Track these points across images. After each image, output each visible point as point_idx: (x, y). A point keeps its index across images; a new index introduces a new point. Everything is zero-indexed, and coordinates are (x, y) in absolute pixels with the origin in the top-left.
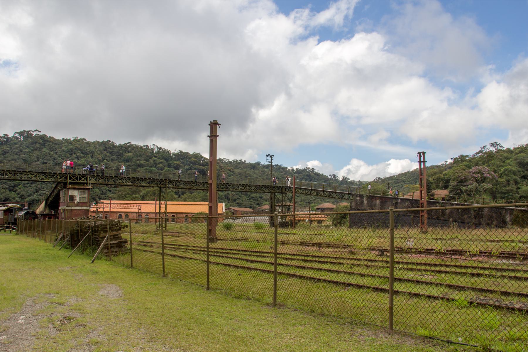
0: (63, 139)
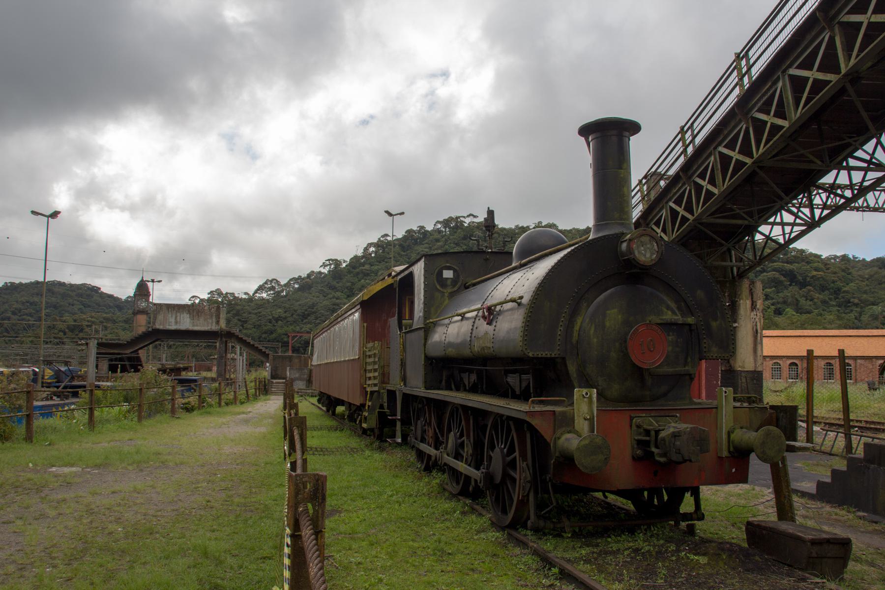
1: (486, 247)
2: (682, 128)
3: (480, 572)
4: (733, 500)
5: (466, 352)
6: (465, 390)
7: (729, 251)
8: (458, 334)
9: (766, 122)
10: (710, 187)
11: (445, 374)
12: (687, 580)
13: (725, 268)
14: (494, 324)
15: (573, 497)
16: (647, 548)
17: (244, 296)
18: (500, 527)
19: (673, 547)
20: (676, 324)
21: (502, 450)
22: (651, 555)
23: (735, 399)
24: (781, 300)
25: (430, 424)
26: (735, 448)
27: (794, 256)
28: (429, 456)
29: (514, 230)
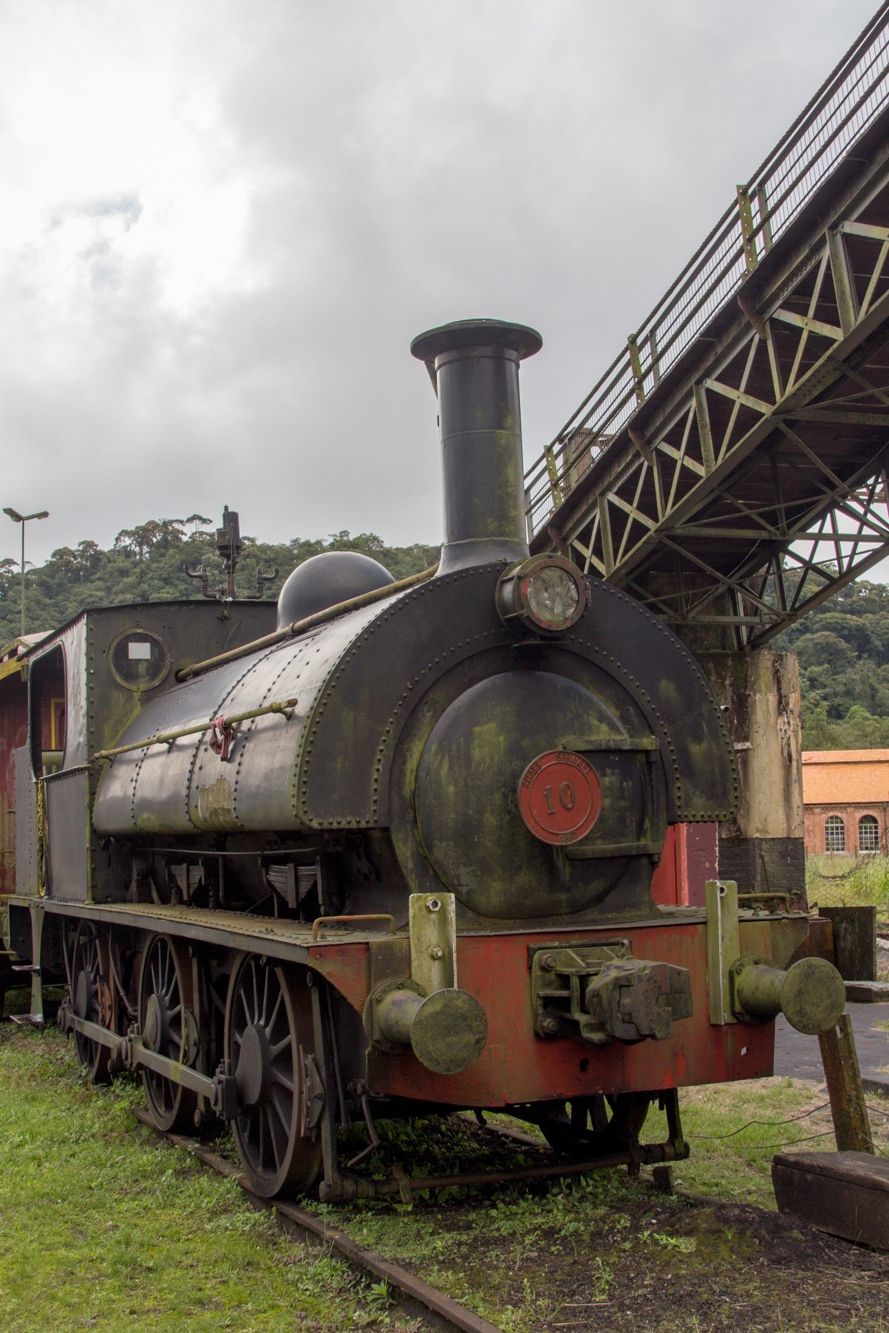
0: (295, 541)
1: (223, 592)
2: (633, 340)
3: (218, 1306)
4: (749, 1110)
5: (180, 822)
6: (181, 902)
7: (731, 592)
8: (162, 781)
9: (800, 330)
10: (690, 463)
11: (136, 868)
12: (654, 1292)
13: (724, 627)
14: (238, 759)
15: (419, 1123)
16: (572, 1227)
18: (261, 1199)
19: (625, 1221)
20: (619, 751)
21: (260, 1031)
22: (579, 1242)
23: (744, 904)
24: (840, 689)
25: (105, 979)
26: (745, 1004)
27: (865, 599)
28: (106, 1051)
29: (289, 550)
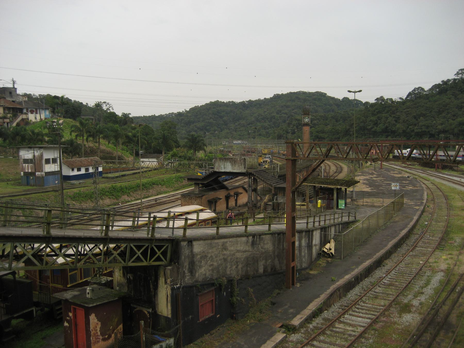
17: (399, 100)
